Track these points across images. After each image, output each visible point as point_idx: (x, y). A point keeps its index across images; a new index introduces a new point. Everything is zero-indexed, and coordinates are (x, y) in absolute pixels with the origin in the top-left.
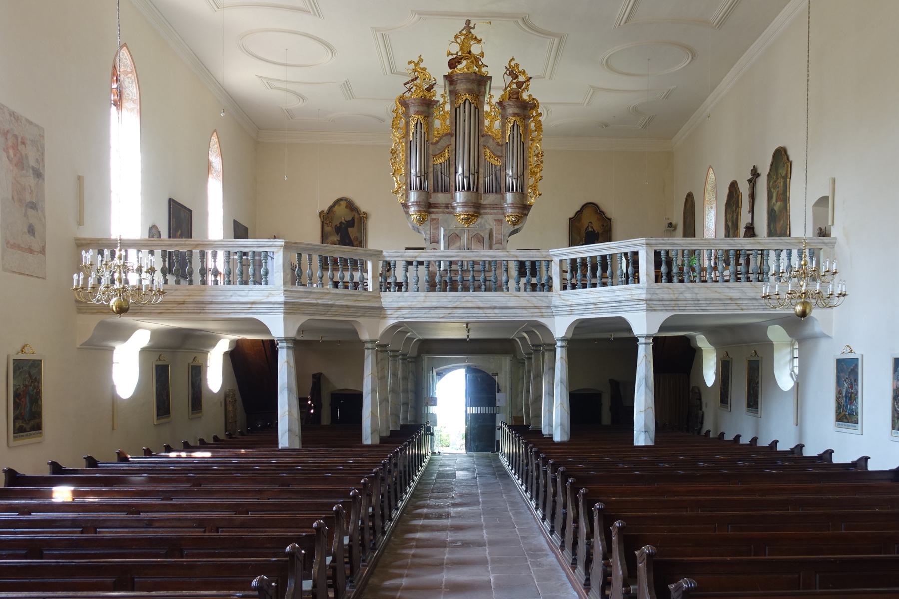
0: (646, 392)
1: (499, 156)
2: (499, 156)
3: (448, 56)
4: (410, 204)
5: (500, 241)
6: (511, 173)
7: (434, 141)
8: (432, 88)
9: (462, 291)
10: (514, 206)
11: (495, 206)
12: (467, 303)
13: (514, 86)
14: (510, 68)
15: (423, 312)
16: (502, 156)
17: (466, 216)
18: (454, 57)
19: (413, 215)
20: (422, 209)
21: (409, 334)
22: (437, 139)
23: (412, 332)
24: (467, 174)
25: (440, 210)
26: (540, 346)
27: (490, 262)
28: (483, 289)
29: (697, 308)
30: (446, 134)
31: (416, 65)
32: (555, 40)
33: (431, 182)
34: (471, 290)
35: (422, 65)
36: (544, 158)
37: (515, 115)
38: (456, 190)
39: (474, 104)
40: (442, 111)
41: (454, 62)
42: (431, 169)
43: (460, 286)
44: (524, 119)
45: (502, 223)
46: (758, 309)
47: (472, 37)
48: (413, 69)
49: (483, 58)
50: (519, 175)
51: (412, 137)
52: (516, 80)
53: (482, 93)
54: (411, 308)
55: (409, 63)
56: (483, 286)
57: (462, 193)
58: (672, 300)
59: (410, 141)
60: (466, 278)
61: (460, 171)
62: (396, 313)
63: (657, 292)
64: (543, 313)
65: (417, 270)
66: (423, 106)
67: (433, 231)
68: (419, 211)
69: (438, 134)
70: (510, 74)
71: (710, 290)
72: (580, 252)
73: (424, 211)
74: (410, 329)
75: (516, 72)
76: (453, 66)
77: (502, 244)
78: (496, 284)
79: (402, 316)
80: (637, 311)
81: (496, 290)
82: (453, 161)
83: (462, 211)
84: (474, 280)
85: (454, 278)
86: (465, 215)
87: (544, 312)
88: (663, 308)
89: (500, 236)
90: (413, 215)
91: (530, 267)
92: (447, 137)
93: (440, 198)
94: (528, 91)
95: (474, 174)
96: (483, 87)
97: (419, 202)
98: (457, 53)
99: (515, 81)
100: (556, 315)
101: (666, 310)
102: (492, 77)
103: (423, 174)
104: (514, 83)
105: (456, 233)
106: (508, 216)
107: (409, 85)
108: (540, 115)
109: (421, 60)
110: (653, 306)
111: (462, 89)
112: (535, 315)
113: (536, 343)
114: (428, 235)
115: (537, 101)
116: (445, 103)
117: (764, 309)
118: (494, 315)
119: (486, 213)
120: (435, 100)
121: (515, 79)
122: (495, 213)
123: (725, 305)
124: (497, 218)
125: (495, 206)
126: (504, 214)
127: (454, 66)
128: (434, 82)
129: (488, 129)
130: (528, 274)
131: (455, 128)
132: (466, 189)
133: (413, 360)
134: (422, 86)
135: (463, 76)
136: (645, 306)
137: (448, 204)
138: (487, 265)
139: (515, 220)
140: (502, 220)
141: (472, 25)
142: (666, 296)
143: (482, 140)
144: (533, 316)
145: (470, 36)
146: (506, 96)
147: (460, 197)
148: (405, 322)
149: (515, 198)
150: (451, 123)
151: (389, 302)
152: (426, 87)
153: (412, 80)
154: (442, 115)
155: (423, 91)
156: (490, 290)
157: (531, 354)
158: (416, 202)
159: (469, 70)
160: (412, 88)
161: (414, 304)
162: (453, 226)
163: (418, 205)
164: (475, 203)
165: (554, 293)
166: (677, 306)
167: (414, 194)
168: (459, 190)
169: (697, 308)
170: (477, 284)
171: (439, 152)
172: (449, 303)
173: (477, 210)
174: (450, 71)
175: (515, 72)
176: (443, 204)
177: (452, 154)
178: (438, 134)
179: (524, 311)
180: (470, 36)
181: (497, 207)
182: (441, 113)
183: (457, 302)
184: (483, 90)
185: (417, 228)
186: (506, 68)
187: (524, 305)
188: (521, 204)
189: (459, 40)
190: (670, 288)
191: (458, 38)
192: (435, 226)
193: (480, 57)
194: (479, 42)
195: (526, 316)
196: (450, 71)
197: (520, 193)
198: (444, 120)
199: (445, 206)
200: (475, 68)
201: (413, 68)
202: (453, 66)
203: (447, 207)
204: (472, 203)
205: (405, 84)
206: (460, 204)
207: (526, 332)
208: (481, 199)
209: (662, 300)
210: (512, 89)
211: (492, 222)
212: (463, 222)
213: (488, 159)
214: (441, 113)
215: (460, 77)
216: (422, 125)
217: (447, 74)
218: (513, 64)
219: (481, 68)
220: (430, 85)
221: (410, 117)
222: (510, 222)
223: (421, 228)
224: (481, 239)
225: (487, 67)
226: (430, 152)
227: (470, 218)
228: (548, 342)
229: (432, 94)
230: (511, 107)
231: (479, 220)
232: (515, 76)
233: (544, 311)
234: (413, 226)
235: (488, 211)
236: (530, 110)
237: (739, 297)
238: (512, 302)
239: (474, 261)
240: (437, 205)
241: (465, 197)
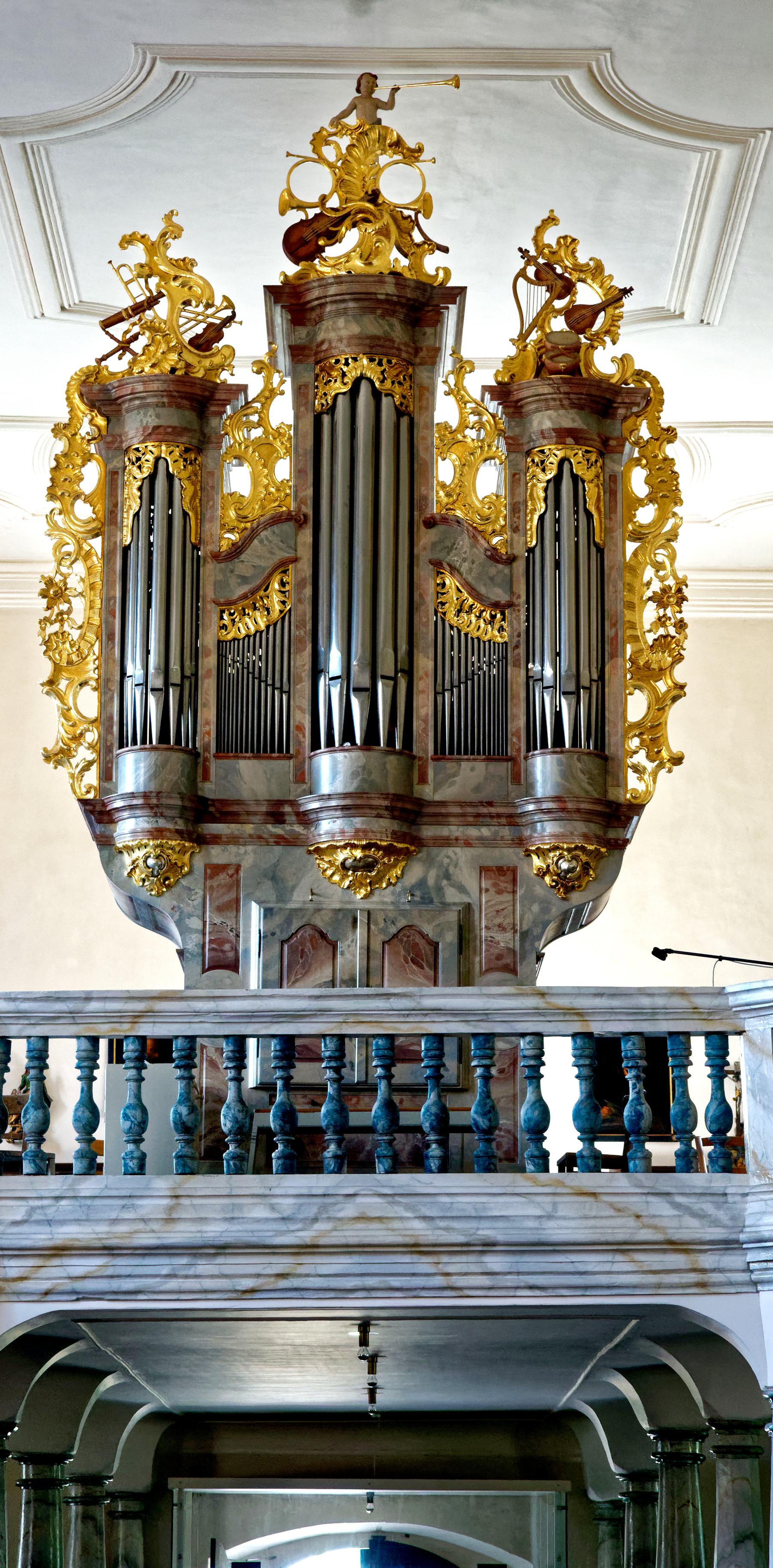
1: (496, 605)
2: (496, 605)
3: (282, 213)
4: (119, 804)
5: (508, 960)
6: (549, 672)
7: (224, 548)
8: (219, 336)
9: (339, 1170)
12: (359, 1225)
13: (558, 324)
14: (540, 253)
15: (163, 1265)
16: (510, 605)
17: (358, 853)
18: (311, 216)
19: (130, 849)
20: (170, 826)
21: (109, 1382)
22: (233, 537)
23: (125, 1373)
24: (360, 678)
25: (249, 829)
26: (699, 1435)
27: (461, 1039)
28: (434, 1164)
30: (277, 520)
31: (152, 248)
32: (718, 157)
33: (208, 713)
34: (379, 1167)
35: (176, 250)
36: (688, 612)
38: (315, 745)
39: (389, 395)
40: (259, 424)
41: (307, 233)
42: (209, 662)
43: (332, 1147)
44: (601, 454)
45: (514, 881)
47: (382, 138)
48: (142, 266)
49: (427, 216)
50: (585, 682)
51: (134, 531)
52: (567, 299)
53: (423, 354)
54: (110, 1250)
55: (127, 241)
56: (434, 1150)
57: (340, 756)
59: (126, 549)
60: (355, 1119)
61: (335, 664)
62: (43, 1273)
64: (703, 1271)
65: (140, 1080)
66: (179, 406)
67: (217, 921)
68: (156, 833)
69: (242, 518)
70: (539, 279)
73: (178, 832)
74: (109, 1351)
75: (565, 268)
76: (303, 251)
77: (514, 971)
78: (489, 1141)
79: (69, 1285)
81: (490, 1168)
82: (301, 625)
83: (342, 832)
84: (394, 1126)
85: (304, 1120)
86: (354, 847)
87: (707, 1266)
89: (504, 939)
90: (130, 849)
91: (643, 1063)
92: (276, 528)
94: (614, 343)
95: (395, 679)
96: (429, 330)
97: (158, 794)
98: (324, 199)
99: (559, 304)
100: (762, 1282)
102: (462, 290)
103: (175, 678)
104: (559, 312)
105: (315, 928)
106: (540, 852)
108: (670, 434)
109: (171, 231)
111: (340, 340)
112: (674, 1278)
113: (676, 1420)
114: (196, 938)
115: (654, 381)
116: (269, 395)
119: (446, 842)
120: (231, 381)
121: (560, 297)
122: (483, 842)
124: (489, 863)
126: (520, 842)
127: (311, 248)
128: (228, 313)
129: (448, 495)
130: (632, 1095)
132: (358, 741)
133: (135, 1506)
134: (175, 329)
135: (344, 288)
137: (280, 803)
138: (451, 1064)
139: (569, 871)
140: (514, 871)
141: (382, 94)
143: (426, 538)
144: (659, 1286)
145: (374, 135)
146: (523, 365)
148: (92, 1318)
149: (566, 773)
150: (298, 472)
151: (15, 1223)
153: (138, 309)
154: (259, 444)
155: (179, 349)
156: (463, 1168)
157: (650, 1476)
158: (146, 795)
159: (370, 264)
160: (135, 338)
161: (123, 1228)
162: (299, 898)
163: (151, 807)
164: (397, 797)
165: (754, 1181)
167: (137, 761)
168: (330, 742)
170: (408, 1148)
171: (245, 589)
172: (282, 1227)
173: (405, 829)
174: (292, 269)
175: (559, 270)
176: (258, 802)
177: (300, 601)
178: (242, 518)
179: (621, 1263)
180: (374, 135)
181: (491, 816)
182: (257, 433)
183: (315, 1220)
184: (429, 342)
185: (150, 907)
186: (524, 252)
187: (620, 1236)
188: (598, 801)
189: (329, 152)
191: (327, 143)
192: (226, 899)
193: (417, 212)
194: (413, 155)
196: (292, 269)
197: (589, 754)
198: (268, 464)
199: (268, 814)
200: (395, 254)
201: (143, 259)
202: (303, 251)
203: (276, 816)
204: (386, 796)
206: (333, 803)
207: (629, 1373)
208: (423, 780)
210: (547, 335)
211: (469, 878)
212: (343, 879)
213: (451, 617)
214: (257, 433)
215: (332, 290)
216: (177, 482)
217: (277, 281)
218: (550, 237)
219: (421, 258)
220: (211, 325)
221: (127, 451)
222: (547, 879)
223: (164, 904)
224: (426, 949)
225: (445, 250)
226: (208, 590)
227: (376, 861)
228: (729, 1411)
229: (217, 360)
230: (544, 403)
231: (416, 872)
232: (560, 283)
233: (707, 1260)
234: (131, 899)
235: (453, 830)
238: (564, 1218)
239: (391, 1038)
240: (235, 808)
241: (354, 774)
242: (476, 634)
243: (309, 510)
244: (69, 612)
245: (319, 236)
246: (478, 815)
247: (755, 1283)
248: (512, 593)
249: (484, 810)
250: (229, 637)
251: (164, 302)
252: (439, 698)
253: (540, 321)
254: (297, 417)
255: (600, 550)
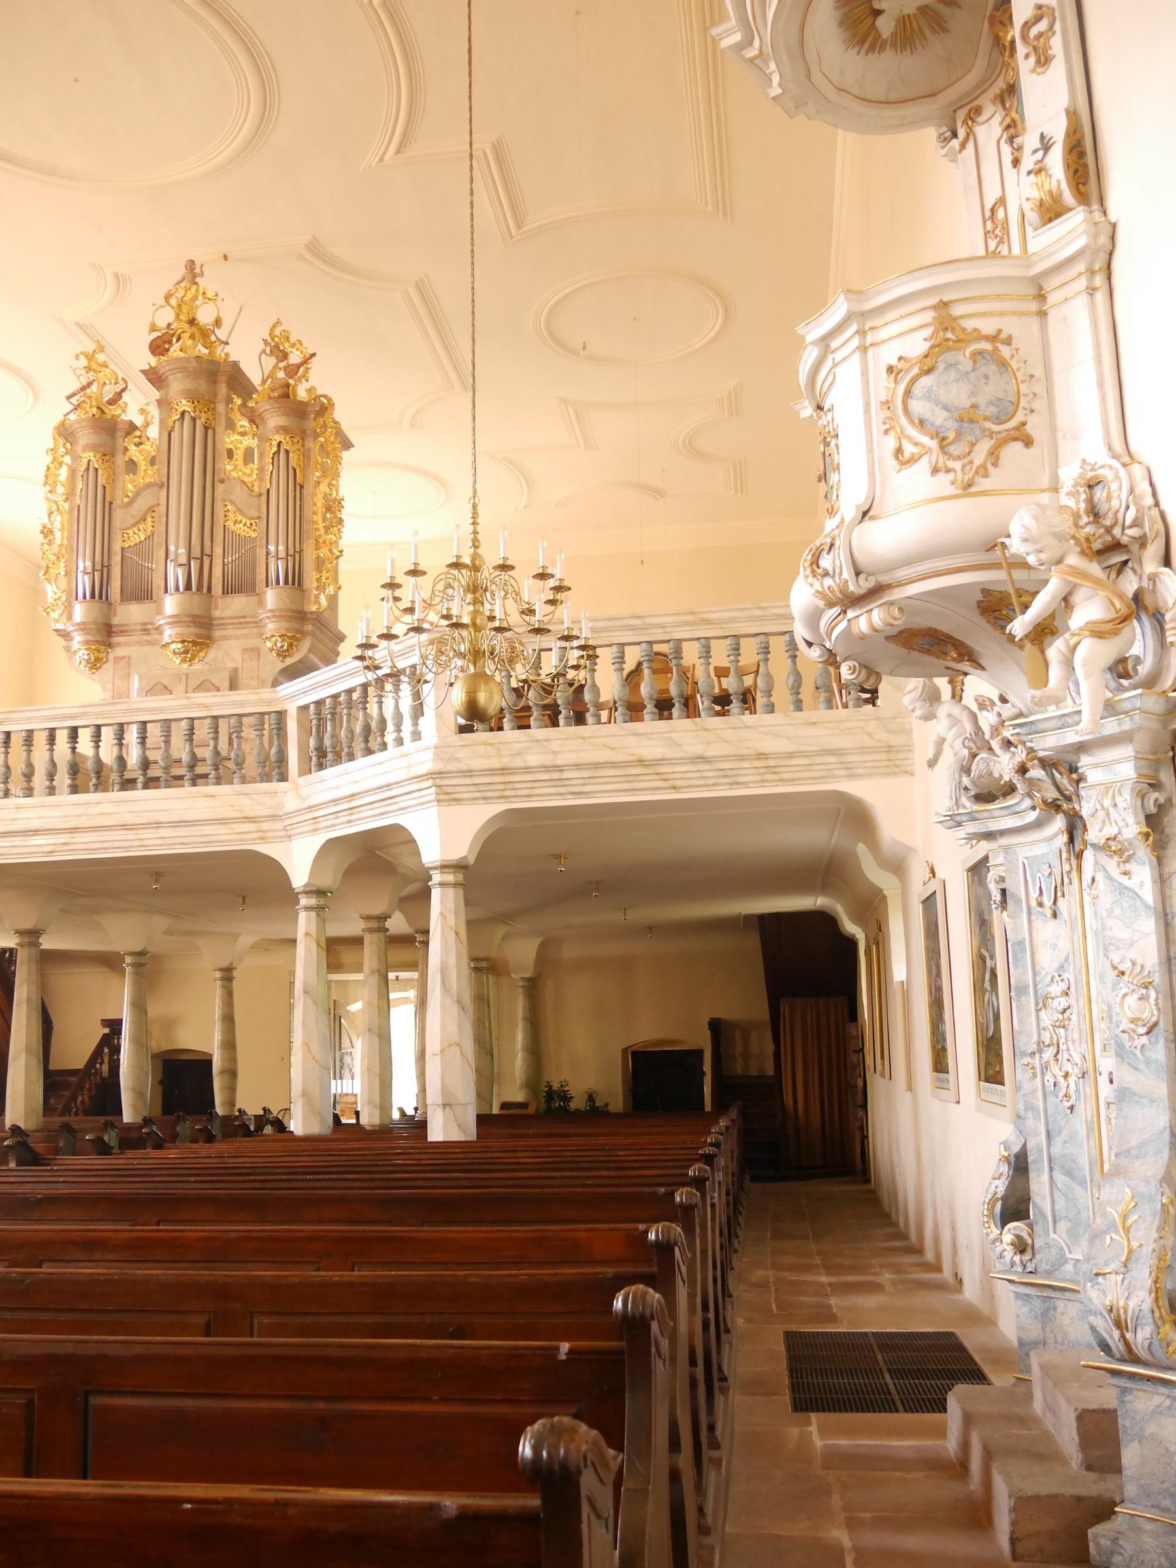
0: (443, 1005)
10: (275, 616)
11: (242, 621)
13: (281, 374)
16: (259, 518)
25: (134, 638)
29: (562, 790)
37: (284, 430)
42: (117, 559)
43: (94, 780)
45: (259, 655)
46: (714, 785)
58: (492, 771)
63: (458, 755)
64: (263, 831)
65: (7, 753)
68: (86, 642)
71: (590, 743)
72: (326, 684)
73: (97, 641)
80: (421, 804)
87: (265, 829)
88: (477, 795)
92: (149, 490)
93: (131, 613)
94: (307, 381)
98: (169, 325)
99: (281, 365)
100: (294, 835)
101: (485, 798)
107: (77, 397)
110: (450, 790)
112: (250, 836)
116: (147, 424)
117: (731, 784)
118: (159, 842)
119: (225, 638)
121: (281, 361)
123: (631, 778)
125: (242, 621)
127: (161, 349)
131: (166, 471)
136: (433, 790)
139: (282, 647)
142: (478, 764)
144: (242, 840)
147: (171, 604)
152: (107, 398)
153: (83, 389)
166: (509, 786)
169: (562, 790)
175: (282, 348)
179: (223, 830)
190: (491, 744)
195: (225, 840)
200: (200, 347)
203: (146, 631)
205: (69, 398)
209: (469, 773)
218: (277, 332)
219: (216, 348)
233: (266, 826)
235: (230, 632)
236: (315, 420)
237: (659, 757)
242: (248, 535)
243: (165, 480)
244: (54, 538)
245: (165, 342)
246: (240, 623)
247: (289, 837)
248: (260, 512)
249: (242, 620)
250: (127, 545)
251: (95, 383)
252: (226, 567)
253: (272, 375)
254: (160, 434)
255: (302, 487)
